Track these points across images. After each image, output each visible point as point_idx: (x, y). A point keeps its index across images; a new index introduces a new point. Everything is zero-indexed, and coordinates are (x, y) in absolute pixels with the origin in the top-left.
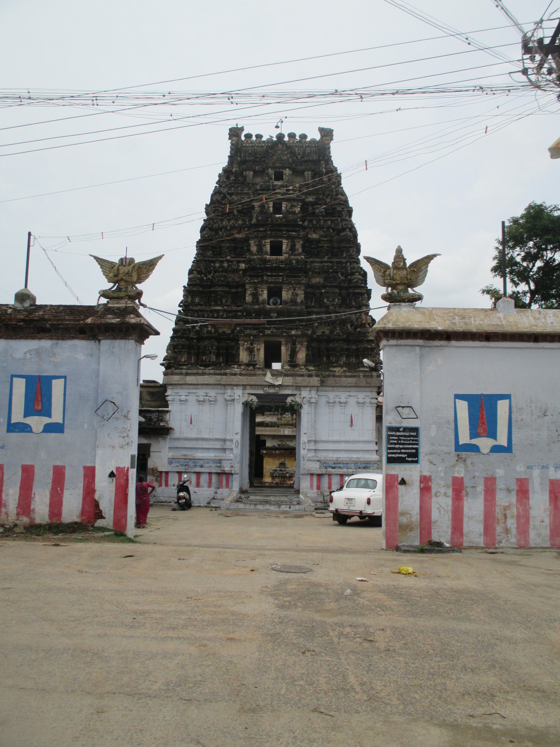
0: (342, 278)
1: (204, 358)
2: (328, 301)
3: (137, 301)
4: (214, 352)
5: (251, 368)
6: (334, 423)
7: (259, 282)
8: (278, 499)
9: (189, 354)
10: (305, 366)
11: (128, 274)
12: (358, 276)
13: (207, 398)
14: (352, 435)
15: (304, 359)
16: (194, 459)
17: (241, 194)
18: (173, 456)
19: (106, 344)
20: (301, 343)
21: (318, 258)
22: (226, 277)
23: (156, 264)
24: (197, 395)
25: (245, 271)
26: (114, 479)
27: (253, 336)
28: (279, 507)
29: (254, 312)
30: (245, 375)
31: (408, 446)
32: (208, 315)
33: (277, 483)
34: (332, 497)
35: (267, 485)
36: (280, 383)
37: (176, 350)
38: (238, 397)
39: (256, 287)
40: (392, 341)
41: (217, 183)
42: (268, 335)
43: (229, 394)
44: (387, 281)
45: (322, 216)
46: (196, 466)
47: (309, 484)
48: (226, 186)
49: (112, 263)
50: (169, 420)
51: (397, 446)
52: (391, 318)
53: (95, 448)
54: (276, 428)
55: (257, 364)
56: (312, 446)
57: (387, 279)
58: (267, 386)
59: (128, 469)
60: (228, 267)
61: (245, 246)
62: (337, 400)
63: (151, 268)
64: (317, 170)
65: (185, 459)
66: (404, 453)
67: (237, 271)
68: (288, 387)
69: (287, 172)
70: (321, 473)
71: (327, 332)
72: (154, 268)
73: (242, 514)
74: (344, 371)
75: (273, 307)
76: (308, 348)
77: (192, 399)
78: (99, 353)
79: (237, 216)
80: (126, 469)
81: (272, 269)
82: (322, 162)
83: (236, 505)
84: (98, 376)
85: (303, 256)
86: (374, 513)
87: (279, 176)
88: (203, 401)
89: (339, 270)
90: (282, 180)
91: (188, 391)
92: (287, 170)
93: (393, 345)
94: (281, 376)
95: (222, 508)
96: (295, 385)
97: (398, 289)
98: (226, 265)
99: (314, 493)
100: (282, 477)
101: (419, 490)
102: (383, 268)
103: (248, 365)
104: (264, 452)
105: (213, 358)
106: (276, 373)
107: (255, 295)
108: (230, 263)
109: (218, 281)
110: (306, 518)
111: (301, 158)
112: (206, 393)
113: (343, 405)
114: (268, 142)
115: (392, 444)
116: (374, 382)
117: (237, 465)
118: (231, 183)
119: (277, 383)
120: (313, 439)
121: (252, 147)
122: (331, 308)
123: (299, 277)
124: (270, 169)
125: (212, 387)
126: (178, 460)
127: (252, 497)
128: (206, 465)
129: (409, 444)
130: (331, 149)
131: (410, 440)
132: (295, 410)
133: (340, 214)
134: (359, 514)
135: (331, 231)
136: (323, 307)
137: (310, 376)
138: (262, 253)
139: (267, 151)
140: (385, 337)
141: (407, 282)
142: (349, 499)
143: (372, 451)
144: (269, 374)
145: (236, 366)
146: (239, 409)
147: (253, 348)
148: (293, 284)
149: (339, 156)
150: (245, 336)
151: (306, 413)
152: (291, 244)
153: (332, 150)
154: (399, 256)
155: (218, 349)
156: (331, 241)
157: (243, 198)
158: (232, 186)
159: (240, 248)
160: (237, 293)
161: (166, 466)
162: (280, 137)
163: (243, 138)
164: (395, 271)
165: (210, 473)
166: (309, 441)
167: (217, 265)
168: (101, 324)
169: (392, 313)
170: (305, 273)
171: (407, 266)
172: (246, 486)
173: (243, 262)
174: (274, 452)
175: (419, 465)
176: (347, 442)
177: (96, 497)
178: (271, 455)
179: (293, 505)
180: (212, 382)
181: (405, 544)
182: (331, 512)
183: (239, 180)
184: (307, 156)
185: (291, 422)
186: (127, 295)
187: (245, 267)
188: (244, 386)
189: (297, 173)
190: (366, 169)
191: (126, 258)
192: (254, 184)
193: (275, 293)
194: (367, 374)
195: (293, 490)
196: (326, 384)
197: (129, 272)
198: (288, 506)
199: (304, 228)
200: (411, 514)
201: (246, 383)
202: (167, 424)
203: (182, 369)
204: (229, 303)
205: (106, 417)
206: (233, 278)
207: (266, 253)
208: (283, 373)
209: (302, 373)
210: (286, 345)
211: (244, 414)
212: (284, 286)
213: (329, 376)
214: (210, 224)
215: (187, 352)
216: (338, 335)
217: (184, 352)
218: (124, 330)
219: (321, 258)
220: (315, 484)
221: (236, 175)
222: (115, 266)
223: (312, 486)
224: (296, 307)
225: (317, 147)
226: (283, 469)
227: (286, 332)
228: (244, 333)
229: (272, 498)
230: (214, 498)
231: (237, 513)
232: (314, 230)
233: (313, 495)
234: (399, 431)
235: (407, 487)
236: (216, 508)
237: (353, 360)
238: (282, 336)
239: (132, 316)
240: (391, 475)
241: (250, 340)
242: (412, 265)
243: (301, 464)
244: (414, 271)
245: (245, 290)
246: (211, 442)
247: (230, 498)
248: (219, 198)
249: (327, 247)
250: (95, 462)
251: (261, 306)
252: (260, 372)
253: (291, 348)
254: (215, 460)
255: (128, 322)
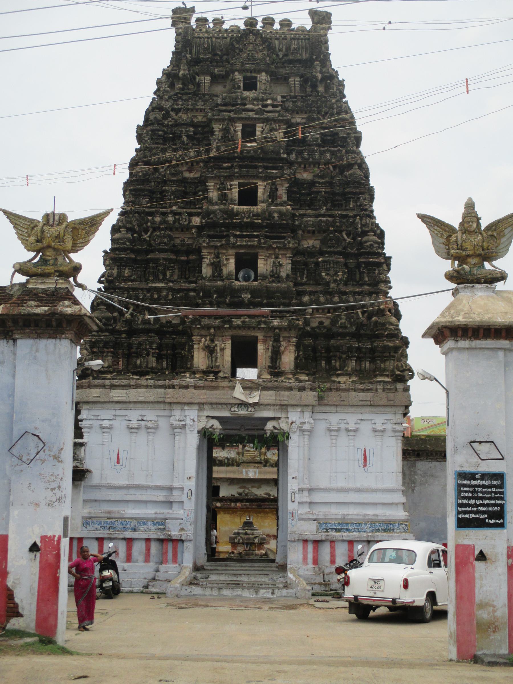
0: (348, 240)
1: (138, 362)
2: (327, 274)
3: (71, 279)
4: (153, 353)
5: (212, 377)
6: (336, 461)
7: (223, 245)
8: (253, 579)
9: (115, 355)
10: (294, 374)
11: (58, 238)
12: (372, 237)
13: (143, 423)
14: (369, 482)
15: (293, 363)
16: (123, 519)
17: (192, 110)
18: (90, 513)
19: (24, 345)
20: (288, 339)
21: (312, 209)
22: (171, 238)
23: (101, 224)
24: (127, 418)
25: (200, 229)
26: (38, 554)
27: (214, 328)
28: (257, 593)
29: (216, 292)
30: (203, 388)
31: (488, 502)
32: (145, 296)
33: (240, 554)
34: (348, 577)
35: (222, 556)
36: (256, 400)
37: (95, 350)
38: (191, 423)
39: (219, 254)
40: (463, 342)
41: (155, 93)
42: (239, 327)
43: (177, 418)
44: (452, 252)
45: (316, 145)
46: (125, 529)
47: (301, 556)
48: (170, 98)
49: (31, 221)
50: (84, 458)
51: (472, 502)
52: (461, 307)
53: (8, 505)
54: (235, 468)
55: (220, 372)
56: (305, 497)
57: (453, 249)
58: (236, 404)
59: (59, 539)
60: (174, 222)
61: (199, 191)
62: (343, 426)
63: (93, 229)
64: (309, 75)
65: (108, 518)
66: (483, 512)
67: (187, 228)
68: (268, 407)
69: (263, 77)
70: (319, 539)
71: (327, 323)
72: (97, 229)
73: (203, 603)
74: (353, 382)
75: (245, 283)
76: (298, 347)
77: (120, 424)
78: (15, 359)
79: (187, 144)
80: (56, 539)
81: (242, 226)
82: (316, 63)
83: (189, 590)
84: (12, 395)
85: (289, 207)
86: (414, 602)
87: (250, 85)
88: (137, 429)
89: (344, 227)
90: (256, 90)
91: (113, 412)
92: (264, 74)
93: (464, 348)
94: (258, 389)
95: (169, 595)
96: (279, 403)
97: (470, 263)
98: (170, 218)
99: (308, 570)
100: (247, 544)
101: (506, 568)
102: (445, 231)
103: (206, 373)
104: (219, 505)
105: (153, 362)
106: (250, 385)
107: (217, 266)
108: (177, 217)
109: (159, 244)
110: (303, 610)
111: (284, 55)
112: (142, 416)
113: (352, 433)
114: (232, 31)
115: (464, 498)
116: (399, 396)
117: (190, 527)
118: (176, 94)
119: (251, 401)
120: (307, 486)
121: (208, 38)
122: (332, 285)
123: (284, 238)
124: (236, 73)
125: (151, 405)
126: (98, 520)
127: (213, 577)
128: (142, 527)
129: (490, 499)
130: (329, 43)
131: (492, 492)
132: (277, 441)
133: (344, 142)
134: (390, 604)
135: (331, 168)
136: (320, 284)
137: (302, 389)
138: (226, 201)
139: (232, 44)
140: (452, 336)
141: (482, 252)
142: (374, 581)
143: (397, 504)
144: (239, 388)
145: (188, 375)
146: (192, 441)
147: (214, 347)
148: (274, 249)
149: (343, 54)
150: (203, 328)
151: (295, 446)
152: (271, 188)
153: (331, 44)
154: (470, 212)
155: (160, 347)
156: (330, 184)
157: (196, 117)
158: (180, 98)
159: (191, 192)
160: (188, 262)
161: (79, 530)
162: (251, 22)
163: (193, 23)
164: (464, 237)
165: (148, 540)
166: (301, 490)
167: (158, 219)
168: (20, 315)
169: (462, 300)
170: (292, 233)
171: (482, 229)
172: (203, 559)
173: (198, 215)
174: (233, 505)
175: (505, 531)
176: (358, 490)
177: (10, 583)
178: (228, 510)
179: (278, 588)
180: (151, 399)
181: (486, 652)
182: (347, 601)
183: (188, 89)
184: (292, 53)
185: (258, 458)
186: (56, 271)
187: (201, 222)
188: (201, 405)
189: (277, 79)
190: (468, 92)
191: (54, 214)
192: (213, 96)
193: (246, 262)
194: (389, 387)
195: (274, 565)
196: (326, 402)
197: (59, 235)
198: (270, 591)
199: (291, 164)
200: (494, 606)
201: (204, 401)
202: (81, 463)
203: (104, 379)
204: (176, 277)
205: (24, 459)
206: (181, 238)
207: (232, 202)
208: (260, 385)
209: (289, 385)
210: (265, 342)
211: (199, 448)
212: (261, 252)
213: (330, 389)
214: (145, 157)
215: (113, 353)
216: (343, 326)
217: (108, 352)
218: (54, 324)
219: (316, 210)
220: (310, 556)
221: (187, 81)
222: (36, 226)
223: (305, 559)
224: (279, 285)
225: (309, 39)
226: (249, 532)
227: (265, 323)
228: (200, 324)
229: (244, 579)
230: (154, 579)
231: (194, 603)
232: (305, 167)
233: (307, 573)
234: (475, 479)
235: (489, 564)
236: (160, 595)
237: (367, 365)
238: (259, 329)
239: (67, 302)
240: (463, 546)
241: (210, 335)
242: (489, 228)
243: (289, 525)
244: (492, 236)
245: (201, 259)
246: (149, 492)
247: (181, 578)
248: (159, 117)
249: (325, 192)
250: (7, 529)
251: (227, 282)
252: (226, 383)
253: (273, 346)
254: (156, 519)
255: (61, 311)
